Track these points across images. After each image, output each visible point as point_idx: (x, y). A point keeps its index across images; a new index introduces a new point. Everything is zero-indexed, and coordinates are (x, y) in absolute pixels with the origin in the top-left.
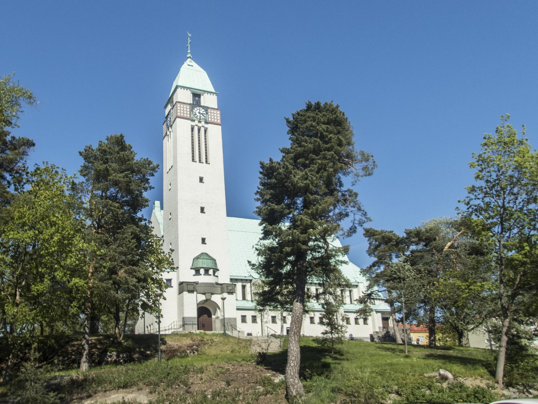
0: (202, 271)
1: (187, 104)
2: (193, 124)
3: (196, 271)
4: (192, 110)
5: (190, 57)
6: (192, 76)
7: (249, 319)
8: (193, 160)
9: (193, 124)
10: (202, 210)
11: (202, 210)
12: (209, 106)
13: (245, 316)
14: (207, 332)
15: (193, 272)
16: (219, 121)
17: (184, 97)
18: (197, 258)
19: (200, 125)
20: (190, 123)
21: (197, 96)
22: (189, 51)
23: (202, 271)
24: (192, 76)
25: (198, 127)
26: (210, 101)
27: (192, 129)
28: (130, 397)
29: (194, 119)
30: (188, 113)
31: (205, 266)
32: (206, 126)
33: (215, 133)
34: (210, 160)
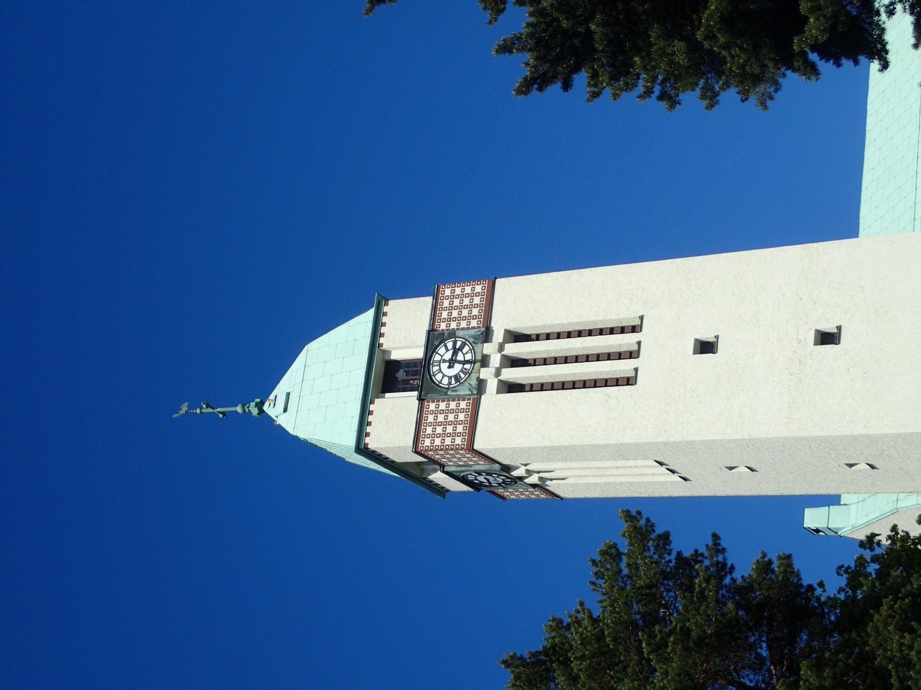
2: (492, 385)
5: (260, 406)
8: (629, 381)
9: (492, 385)
16: (478, 289)
17: (395, 424)
19: (495, 360)
20: (491, 399)
22: (239, 409)
24: (320, 395)
26: (406, 327)
29: (474, 382)
32: (498, 336)
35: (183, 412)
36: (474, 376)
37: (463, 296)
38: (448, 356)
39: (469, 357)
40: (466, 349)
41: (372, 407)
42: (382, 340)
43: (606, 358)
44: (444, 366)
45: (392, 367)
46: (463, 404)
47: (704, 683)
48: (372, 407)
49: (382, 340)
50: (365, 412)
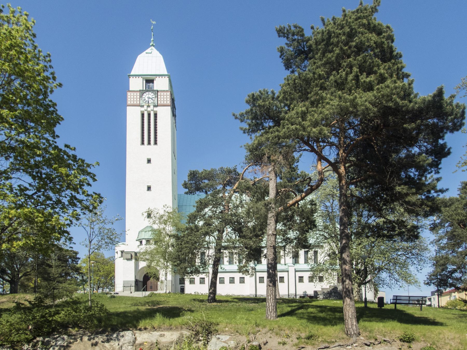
0: (144, 242)
1: (137, 91)
2: (143, 109)
3: (147, 241)
4: (141, 96)
5: (152, 45)
6: (150, 62)
7: (237, 280)
8: (143, 143)
9: (143, 109)
10: (149, 188)
11: (149, 188)
12: (158, 90)
13: (302, 277)
14: (155, 292)
15: (138, 243)
16: (168, 102)
17: (136, 84)
18: (142, 231)
19: (149, 109)
20: (139, 109)
21: (149, 81)
22: (152, 39)
23: (144, 242)
24: (150, 62)
25: (148, 111)
26: (162, 84)
27: (143, 115)
28: (143, 337)
29: (143, 104)
30: (138, 100)
31: (147, 237)
32: (155, 109)
33: (165, 115)
34: (158, 142)
35: (152, 22)
36: (145, 104)
37: (131, 98)
38: (151, 97)
39: (150, 102)
40: (152, 101)
41: (140, 77)
42: (158, 77)
43: (149, 135)
44: (147, 96)
45: (152, 81)
46: (165, 102)
47: (219, 191)
48: (140, 77)
49: (158, 77)
50: (139, 76)
